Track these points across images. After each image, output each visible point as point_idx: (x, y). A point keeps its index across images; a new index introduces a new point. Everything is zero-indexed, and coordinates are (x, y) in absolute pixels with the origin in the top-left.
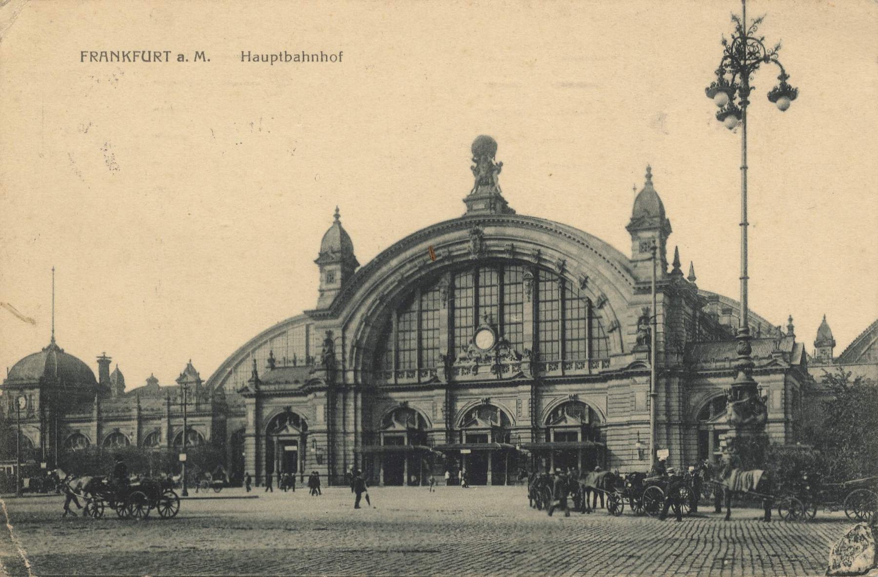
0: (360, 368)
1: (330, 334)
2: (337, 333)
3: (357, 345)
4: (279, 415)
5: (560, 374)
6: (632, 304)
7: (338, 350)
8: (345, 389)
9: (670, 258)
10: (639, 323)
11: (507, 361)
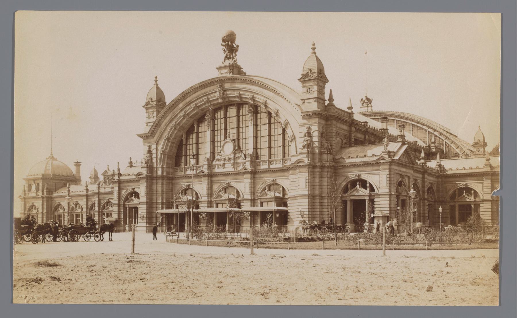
0: (165, 166)
1: (150, 147)
2: (154, 146)
3: (164, 153)
4: (129, 193)
5: (267, 167)
6: (301, 125)
7: (154, 156)
8: (157, 178)
9: (327, 97)
10: (305, 136)
11: (239, 161)
